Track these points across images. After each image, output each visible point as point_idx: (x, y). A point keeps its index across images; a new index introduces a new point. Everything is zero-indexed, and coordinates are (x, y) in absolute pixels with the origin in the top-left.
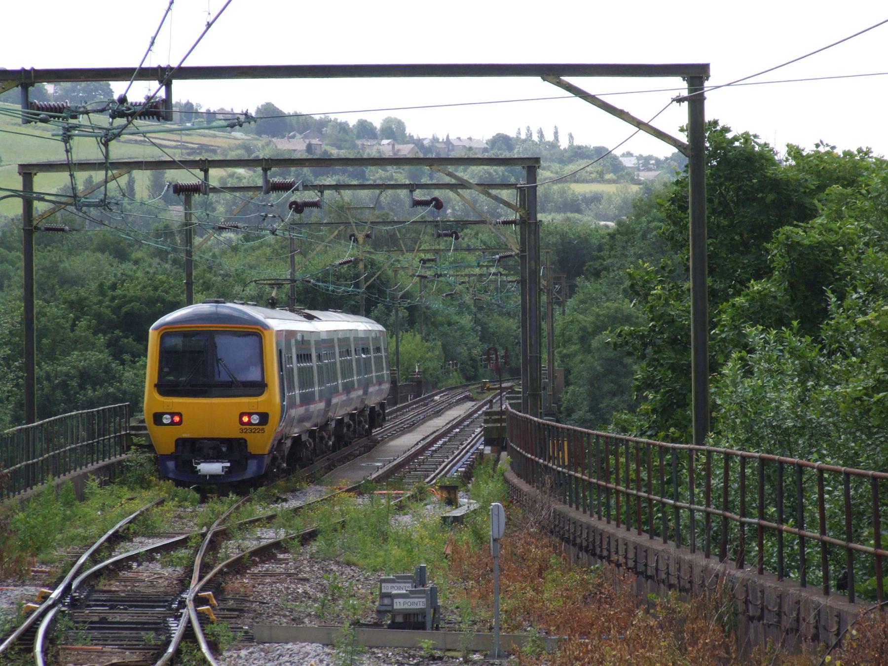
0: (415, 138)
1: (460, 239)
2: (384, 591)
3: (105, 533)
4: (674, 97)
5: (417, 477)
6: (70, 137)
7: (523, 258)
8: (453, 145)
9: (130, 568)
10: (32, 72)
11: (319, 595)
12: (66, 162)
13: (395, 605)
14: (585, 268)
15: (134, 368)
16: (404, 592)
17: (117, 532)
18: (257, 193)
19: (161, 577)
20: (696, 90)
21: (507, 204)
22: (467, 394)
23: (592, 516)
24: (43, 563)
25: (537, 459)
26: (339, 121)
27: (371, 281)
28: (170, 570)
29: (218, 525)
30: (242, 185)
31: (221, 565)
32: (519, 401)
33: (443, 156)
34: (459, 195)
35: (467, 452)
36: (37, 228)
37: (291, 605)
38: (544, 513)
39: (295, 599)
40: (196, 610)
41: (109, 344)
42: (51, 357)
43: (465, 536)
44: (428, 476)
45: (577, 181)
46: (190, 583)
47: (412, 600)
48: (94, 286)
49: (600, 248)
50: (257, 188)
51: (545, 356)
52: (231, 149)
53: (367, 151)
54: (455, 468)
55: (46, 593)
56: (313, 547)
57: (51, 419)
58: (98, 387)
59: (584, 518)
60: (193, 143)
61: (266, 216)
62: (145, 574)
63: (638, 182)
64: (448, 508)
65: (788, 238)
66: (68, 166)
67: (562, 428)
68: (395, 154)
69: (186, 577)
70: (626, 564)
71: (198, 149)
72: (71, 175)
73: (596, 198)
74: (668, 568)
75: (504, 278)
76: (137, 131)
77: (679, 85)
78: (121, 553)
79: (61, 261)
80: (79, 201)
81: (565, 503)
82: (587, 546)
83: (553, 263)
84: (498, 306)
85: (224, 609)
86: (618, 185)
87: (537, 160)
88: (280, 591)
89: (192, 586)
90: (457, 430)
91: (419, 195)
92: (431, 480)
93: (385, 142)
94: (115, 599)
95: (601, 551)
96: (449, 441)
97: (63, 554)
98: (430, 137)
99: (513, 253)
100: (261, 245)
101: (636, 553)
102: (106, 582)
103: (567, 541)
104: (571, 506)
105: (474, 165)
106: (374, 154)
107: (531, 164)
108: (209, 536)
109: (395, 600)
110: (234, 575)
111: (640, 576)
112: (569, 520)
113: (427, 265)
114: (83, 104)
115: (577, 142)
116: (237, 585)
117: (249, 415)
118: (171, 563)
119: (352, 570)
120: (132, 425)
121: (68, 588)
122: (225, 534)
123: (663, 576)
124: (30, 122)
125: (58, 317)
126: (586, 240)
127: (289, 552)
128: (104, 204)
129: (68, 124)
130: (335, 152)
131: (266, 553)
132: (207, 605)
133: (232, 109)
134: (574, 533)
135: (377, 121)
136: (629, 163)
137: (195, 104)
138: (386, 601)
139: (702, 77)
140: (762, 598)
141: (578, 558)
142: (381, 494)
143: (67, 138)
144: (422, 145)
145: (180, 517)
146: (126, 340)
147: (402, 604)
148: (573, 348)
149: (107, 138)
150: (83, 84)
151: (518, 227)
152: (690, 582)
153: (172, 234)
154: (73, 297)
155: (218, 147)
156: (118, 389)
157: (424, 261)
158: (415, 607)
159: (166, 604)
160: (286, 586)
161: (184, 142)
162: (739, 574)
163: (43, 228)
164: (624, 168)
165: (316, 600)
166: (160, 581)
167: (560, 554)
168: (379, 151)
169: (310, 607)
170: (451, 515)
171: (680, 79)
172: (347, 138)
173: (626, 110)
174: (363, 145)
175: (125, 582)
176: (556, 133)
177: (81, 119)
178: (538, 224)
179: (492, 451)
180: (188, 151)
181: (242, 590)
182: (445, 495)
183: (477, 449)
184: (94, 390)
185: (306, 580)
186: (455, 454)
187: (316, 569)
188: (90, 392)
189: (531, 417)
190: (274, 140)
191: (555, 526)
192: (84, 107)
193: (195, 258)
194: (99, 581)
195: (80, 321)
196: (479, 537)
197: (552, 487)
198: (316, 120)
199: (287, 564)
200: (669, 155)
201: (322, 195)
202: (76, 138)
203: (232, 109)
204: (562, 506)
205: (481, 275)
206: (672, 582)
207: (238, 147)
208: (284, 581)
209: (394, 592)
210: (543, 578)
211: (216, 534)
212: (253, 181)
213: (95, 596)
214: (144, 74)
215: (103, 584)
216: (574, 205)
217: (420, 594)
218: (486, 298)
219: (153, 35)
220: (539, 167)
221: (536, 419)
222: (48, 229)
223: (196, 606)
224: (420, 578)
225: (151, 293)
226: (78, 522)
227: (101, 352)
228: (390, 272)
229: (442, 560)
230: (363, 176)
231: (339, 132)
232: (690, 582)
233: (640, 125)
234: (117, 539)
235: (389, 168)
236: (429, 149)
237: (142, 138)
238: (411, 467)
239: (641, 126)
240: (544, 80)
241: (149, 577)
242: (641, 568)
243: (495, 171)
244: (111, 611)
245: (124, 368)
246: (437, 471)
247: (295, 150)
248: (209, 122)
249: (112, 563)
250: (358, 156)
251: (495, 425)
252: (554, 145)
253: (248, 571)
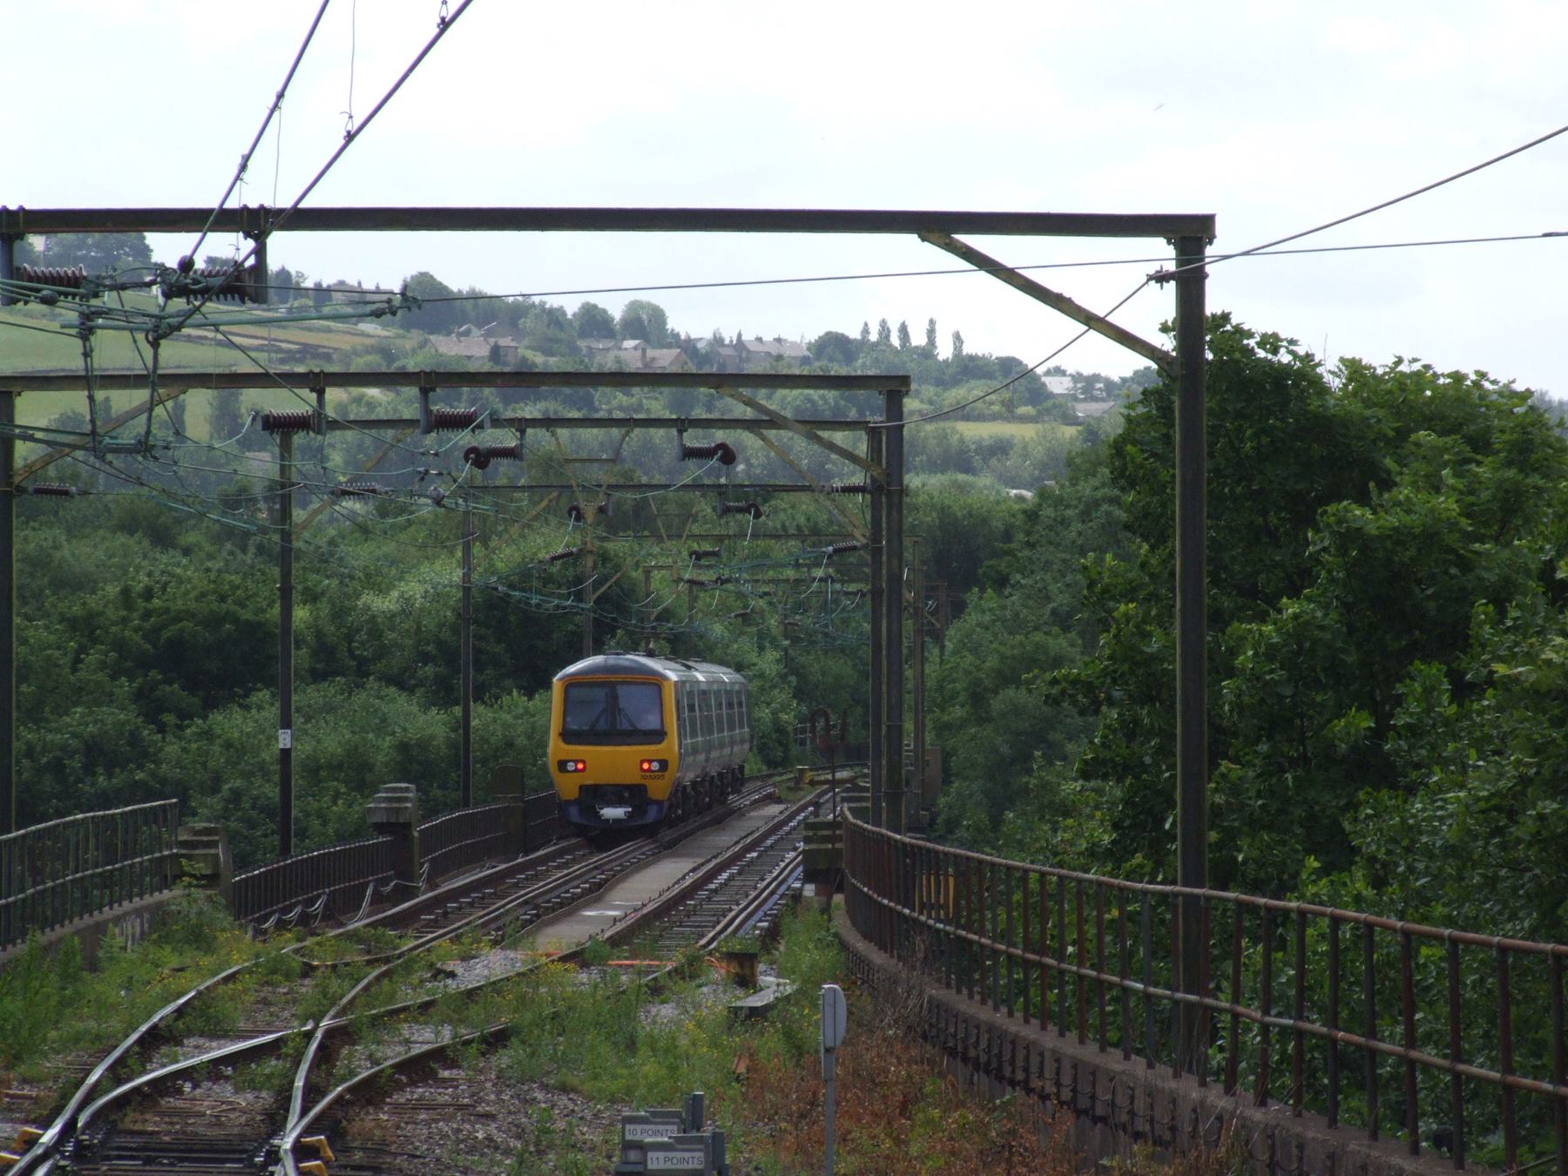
0: (683, 337)
1: (763, 518)
2: (628, 1137)
3: (135, 1029)
4: (1152, 272)
5: (683, 936)
6: (91, 330)
7: (876, 552)
8: (749, 352)
9: (180, 1091)
10: (21, 214)
11: (513, 1143)
12: (83, 373)
13: (649, 1162)
14: (980, 571)
15: (180, 738)
16: (666, 1139)
17: (155, 1027)
18: (409, 431)
19: (234, 1109)
20: (1189, 262)
21: (853, 458)
22: (770, 790)
23: (996, 1009)
24: (25, 1081)
25: (899, 907)
26: (547, 306)
27: (602, 590)
28: (250, 1096)
29: (334, 1017)
30: (373, 417)
31: (340, 1089)
32: (864, 804)
33: (730, 370)
34: (763, 439)
35: (772, 893)
36: (21, 490)
37: (462, 1160)
38: (911, 1003)
39: (471, 1151)
40: (297, 1168)
41: (139, 696)
42: (34, 716)
43: (770, 1042)
44: (702, 936)
45: (967, 418)
46: (285, 1119)
47: (679, 1155)
48: (113, 590)
49: (1007, 536)
50: (411, 423)
51: (909, 726)
52: (355, 352)
53: (598, 359)
54: (751, 922)
55: (31, 1134)
56: (503, 1058)
57: (40, 826)
58: (117, 770)
59: (984, 1014)
60: (289, 342)
61: (427, 472)
62: (206, 1103)
63: (1074, 421)
64: (740, 992)
65: (1340, 522)
66: (87, 380)
67: (946, 854)
68: (646, 365)
69: (279, 1108)
70: (1058, 1095)
71: (299, 351)
72: (91, 398)
73: (1000, 448)
74: (1132, 1103)
75: (838, 586)
76: (204, 321)
77: (1160, 252)
78: (164, 1066)
79: (56, 547)
80: (100, 442)
81: (948, 986)
82: (988, 1063)
83: (923, 562)
84: (826, 635)
85: (345, 1167)
86: (1039, 426)
87: (905, 380)
88: (445, 1136)
89: (290, 1125)
90: (755, 854)
91: (693, 438)
92: (710, 943)
93: (629, 344)
94: (154, 1146)
95: (1013, 1072)
96: (740, 873)
97: (60, 1065)
98: (708, 335)
99: (858, 544)
100: (410, 523)
101: (1075, 1076)
102: (138, 1116)
103: (952, 1053)
104: (959, 991)
105: (786, 387)
106: (609, 365)
107: (892, 386)
108: (319, 1035)
110: (362, 1107)
111: (1083, 1118)
112: (956, 1016)
113: (703, 562)
114: (111, 272)
115: (969, 349)
116: (369, 1125)
117: (650, 762)
118: (253, 1086)
119: (570, 1099)
120: (181, 838)
121: (70, 1127)
122: (347, 1034)
123: (1124, 1118)
124: (14, 301)
125: (49, 647)
126: (984, 521)
127: (459, 1067)
128: (144, 447)
129: (88, 307)
130: (539, 361)
131: (419, 1068)
132: (316, 1159)
133: (360, 283)
134: (964, 1040)
135: (615, 308)
136: (1057, 386)
137: (293, 273)
138: (633, 1156)
139: (1200, 239)
140: (1301, 1159)
141: (972, 1083)
142: (621, 966)
143: (86, 332)
144: (695, 350)
145: (265, 1002)
146: (168, 688)
147: (662, 1161)
148: (958, 712)
149: (160, 330)
150: (97, 236)
151: (868, 497)
152: (1173, 1129)
153: (253, 501)
154: (76, 610)
155: (334, 349)
156: (153, 774)
157: (699, 556)
158: (685, 1166)
159: (244, 1156)
160: (455, 1126)
161: (276, 340)
162: (1257, 1115)
163: (30, 489)
164: (1051, 395)
165: (508, 1152)
166: (232, 1116)
167: (941, 1075)
168: (618, 360)
169: (499, 1164)
170: (744, 1004)
171: (1161, 241)
172: (563, 336)
173: (1067, 295)
174: (590, 348)
175: (170, 1116)
176: (931, 333)
177: (106, 299)
178: (903, 491)
180: (279, 356)
181: (378, 1133)
182: (735, 968)
183: (789, 888)
184: (110, 776)
185: (489, 1117)
186: (750, 898)
187: (507, 1098)
188: (101, 779)
189: (889, 833)
190: (432, 338)
191: (931, 1026)
192: (111, 277)
193: (297, 544)
194: (125, 1115)
195: (88, 654)
196: (798, 1049)
197: (925, 958)
198: (508, 304)
199: (456, 1087)
200: (1128, 374)
201: (522, 438)
202: (99, 332)
203: (360, 283)
204: (942, 992)
205: (798, 582)
206: (1140, 1129)
207: (369, 350)
208: (452, 1118)
209: (648, 1140)
210: (909, 1118)
211: (330, 1033)
212: (395, 410)
213: (120, 1140)
214: (224, 219)
215: (131, 1120)
216: (961, 460)
217: (691, 1143)
218: (806, 621)
219: (246, 152)
220: (907, 393)
221: (898, 837)
222: (38, 491)
223: (297, 1160)
224: (694, 1115)
225: (215, 606)
226: (86, 1010)
227: (123, 708)
228: (637, 574)
229: (729, 1084)
230: (589, 403)
231: (548, 325)
232: (1173, 1129)
233: (1092, 321)
234: (155, 1040)
235: (636, 390)
236: (705, 358)
237: (211, 335)
238: (674, 919)
239: (1092, 323)
240: (923, 240)
241: (213, 1108)
242: (1083, 1103)
243: (822, 397)
244: (147, 1168)
245: (164, 738)
246: (718, 928)
247: (469, 358)
248: (317, 307)
249: (148, 1083)
250: (581, 369)
251: (824, 846)
252: (928, 352)
253: (388, 1100)
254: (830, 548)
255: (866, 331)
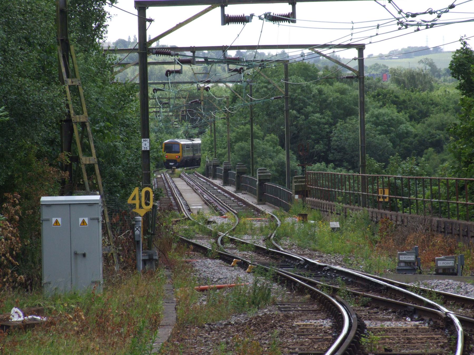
2: (401, 259)
47: (447, 262)
109: (439, 262)
158: (449, 265)
179: (299, 197)
182: (301, 218)
203: (151, 21)
251: (300, 184)
254: (273, 98)
255: (129, 38)
